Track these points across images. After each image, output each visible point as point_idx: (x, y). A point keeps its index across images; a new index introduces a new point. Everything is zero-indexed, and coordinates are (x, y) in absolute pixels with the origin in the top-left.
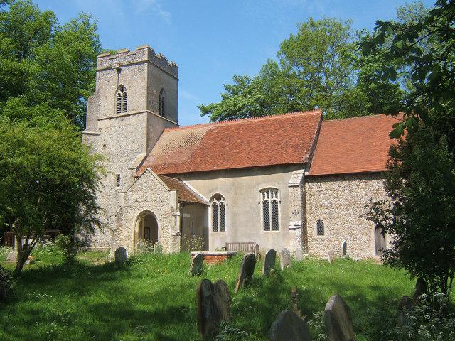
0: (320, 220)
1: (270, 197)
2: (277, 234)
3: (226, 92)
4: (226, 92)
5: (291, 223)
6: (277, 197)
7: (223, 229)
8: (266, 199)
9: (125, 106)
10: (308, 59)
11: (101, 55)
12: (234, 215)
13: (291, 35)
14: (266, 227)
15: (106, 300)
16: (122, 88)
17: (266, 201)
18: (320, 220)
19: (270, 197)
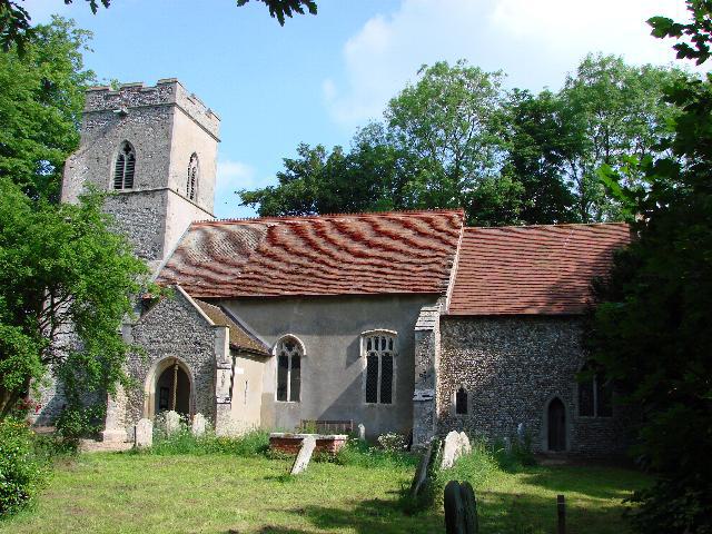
0: (462, 390)
1: (380, 347)
2: (389, 409)
3: (284, 170)
4: (284, 170)
5: (416, 392)
6: (391, 348)
7: (295, 397)
8: (373, 350)
9: (130, 178)
10: (507, 139)
11: (400, 216)
12: (316, 374)
13: (284, 159)
14: (371, 397)
15: (236, 230)
16: (128, 148)
17: (373, 354)
18: (462, 390)
19: (380, 347)
